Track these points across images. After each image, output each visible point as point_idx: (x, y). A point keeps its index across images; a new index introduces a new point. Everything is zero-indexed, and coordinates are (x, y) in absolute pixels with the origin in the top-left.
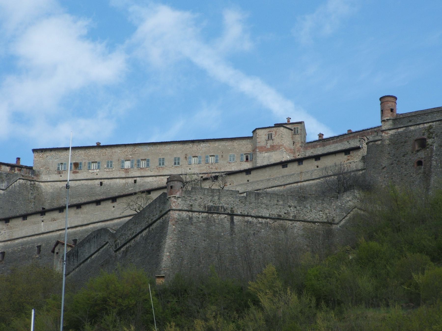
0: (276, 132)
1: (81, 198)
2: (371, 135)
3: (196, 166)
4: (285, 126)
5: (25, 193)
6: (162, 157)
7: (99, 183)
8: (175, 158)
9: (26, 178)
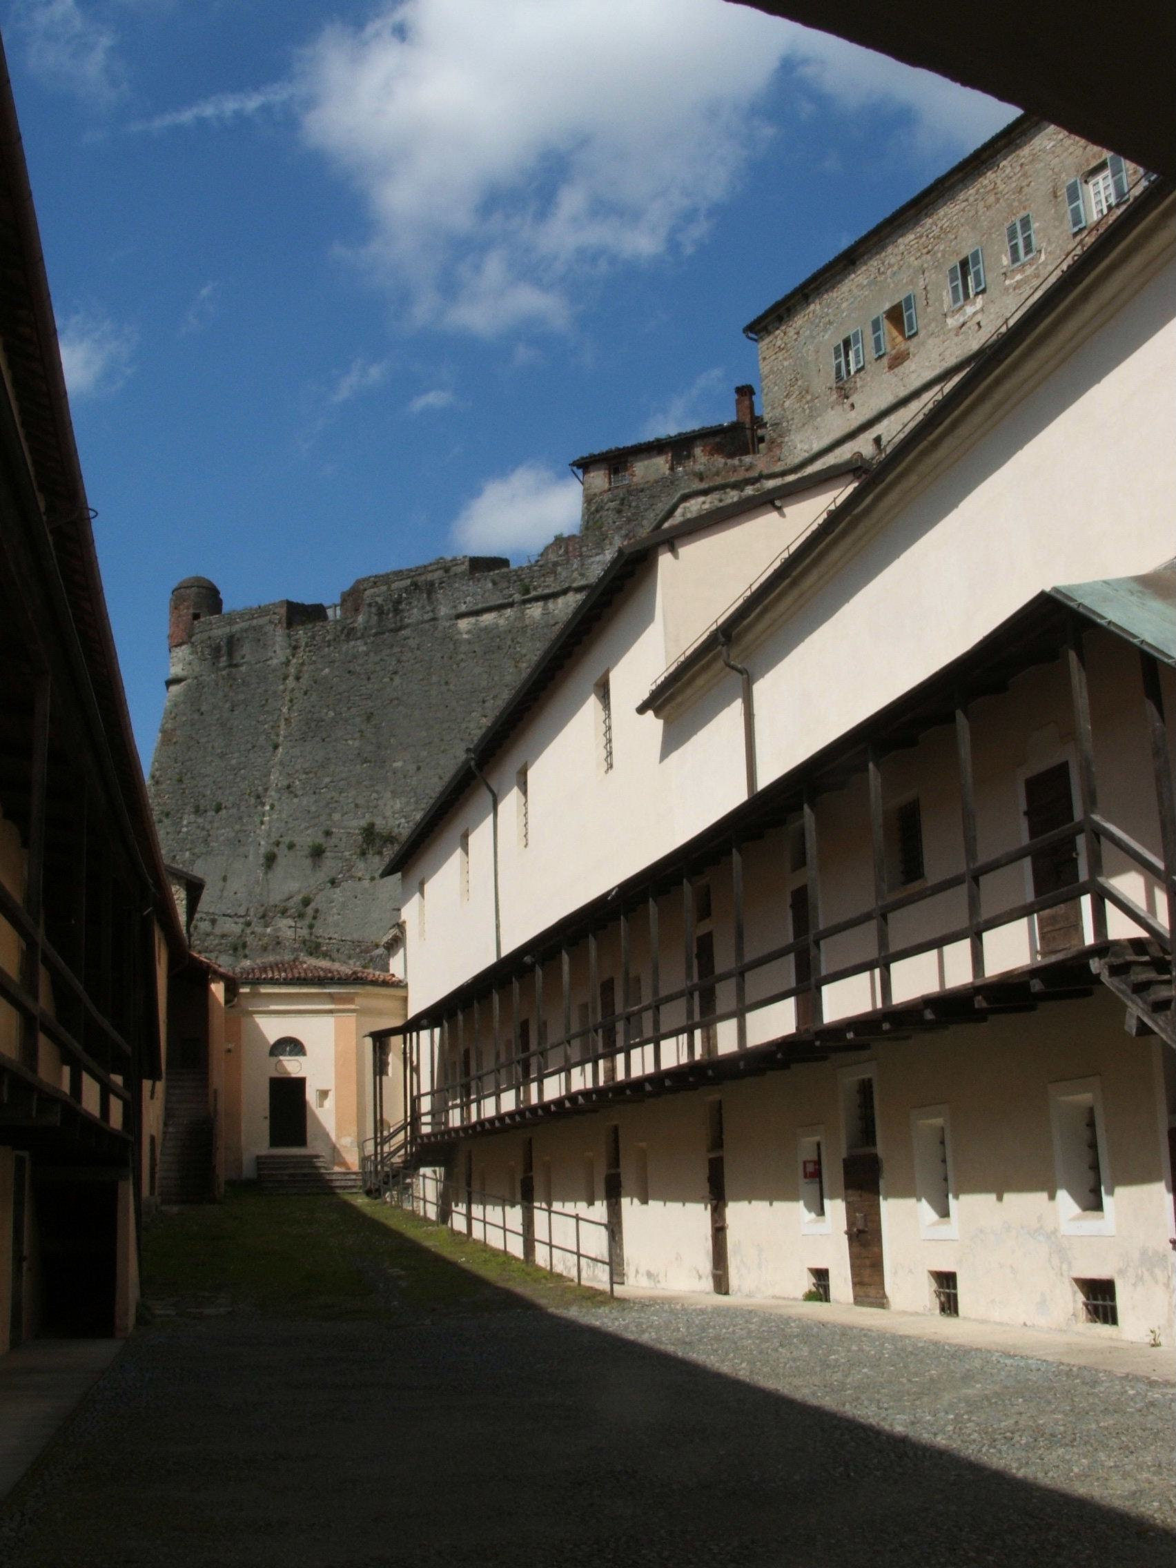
9: (719, 481)
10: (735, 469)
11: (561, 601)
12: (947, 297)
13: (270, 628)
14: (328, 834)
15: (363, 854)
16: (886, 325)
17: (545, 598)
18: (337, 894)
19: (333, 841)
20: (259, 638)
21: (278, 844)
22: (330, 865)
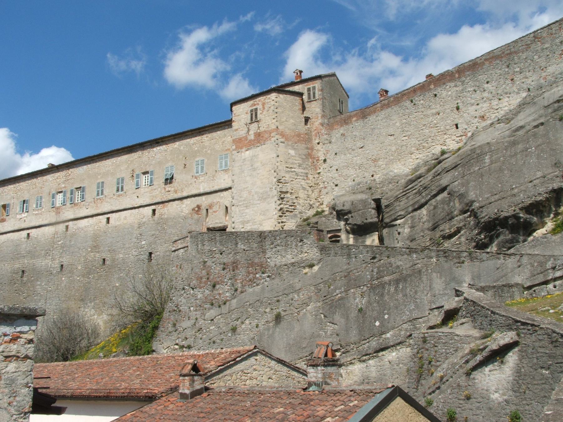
0: (263, 104)
2: (459, 77)
3: (147, 190)
4: (291, 89)
6: (101, 181)
7: (26, 235)
8: (99, 183)
12: (18, 209)
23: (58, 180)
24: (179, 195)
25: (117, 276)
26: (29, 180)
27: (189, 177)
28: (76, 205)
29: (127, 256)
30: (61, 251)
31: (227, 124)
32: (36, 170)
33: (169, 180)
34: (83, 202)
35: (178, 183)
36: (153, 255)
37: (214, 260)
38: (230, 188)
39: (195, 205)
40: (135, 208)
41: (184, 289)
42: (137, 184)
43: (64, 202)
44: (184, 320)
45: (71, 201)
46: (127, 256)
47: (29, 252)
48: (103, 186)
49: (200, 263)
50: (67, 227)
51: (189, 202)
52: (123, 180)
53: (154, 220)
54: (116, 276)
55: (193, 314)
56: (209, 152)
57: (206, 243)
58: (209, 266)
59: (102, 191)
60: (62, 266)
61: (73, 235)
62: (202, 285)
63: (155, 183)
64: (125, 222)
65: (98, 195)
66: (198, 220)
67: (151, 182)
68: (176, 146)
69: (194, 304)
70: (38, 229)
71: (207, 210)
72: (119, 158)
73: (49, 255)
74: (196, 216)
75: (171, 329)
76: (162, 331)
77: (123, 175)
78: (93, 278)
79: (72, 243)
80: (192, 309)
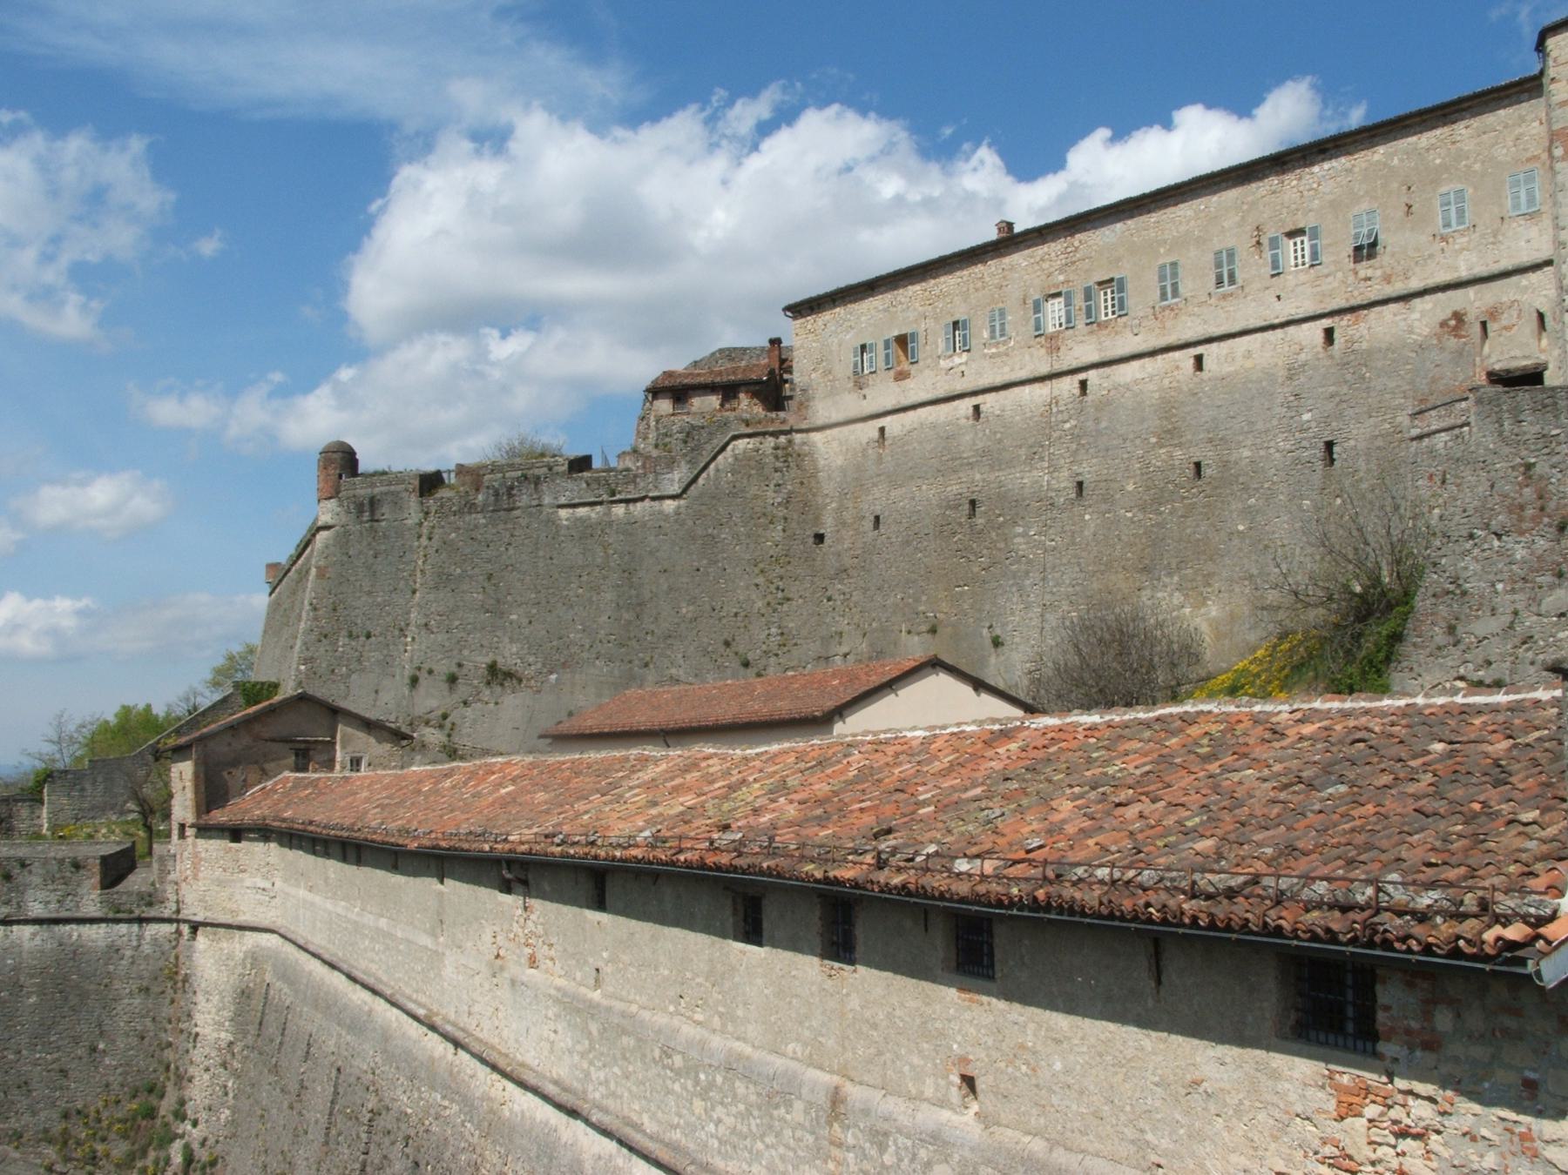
1: (919, 482)
3: (1303, 277)
5: (753, 490)
6: (1169, 260)
7: (971, 410)
8: (1163, 267)
9: (760, 429)
10: (772, 421)
11: (639, 505)
12: (942, 345)
13: (405, 495)
14: (460, 665)
15: (488, 683)
16: (894, 345)
17: (627, 501)
18: (469, 712)
19: (465, 671)
20: (397, 503)
21: (419, 669)
22: (463, 690)
23: (1046, 265)
24: (1398, 288)
25: (1240, 506)
26: (961, 269)
27: (1424, 238)
28: (1102, 326)
29: (1262, 453)
30: (1074, 446)
31: (1530, 87)
32: (980, 242)
33: (1366, 251)
34: (1124, 319)
35: (1393, 255)
36: (1336, 449)
37: (1555, 459)
38: (1549, 263)
39: (1449, 313)
40: (1273, 327)
41: (1471, 536)
42: (1275, 264)
43: (1068, 321)
44: (1477, 617)
45: (1089, 315)
46: (1262, 453)
47: (985, 453)
48: (1175, 275)
49: (1513, 468)
50: (1083, 384)
51: (1429, 306)
52: (1231, 254)
53: (1332, 357)
54: (1236, 505)
55: (1505, 602)
56: (1477, 167)
57: (1527, 416)
58: (1541, 477)
59: (1175, 287)
60: (1080, 484)
61: (1104, 404)
62: (1525, 526)
63: (1324, 258)
64: (1249, 364)
65: (1164, 296)
66: (1460, 353)
67: (1314, 255)
68: (1376, 157)
69: (1506, 576)
70: (1002, 393)
71: (1484, 324)
72: (1215, 198)
73: (1042, 459)
74: (1453, 341)
75: (1440, 637)
76: (1414, 645)
77: (1230, 242)
78: (1171, 513)
79: (1104, 424)
80: (1500, 586)
